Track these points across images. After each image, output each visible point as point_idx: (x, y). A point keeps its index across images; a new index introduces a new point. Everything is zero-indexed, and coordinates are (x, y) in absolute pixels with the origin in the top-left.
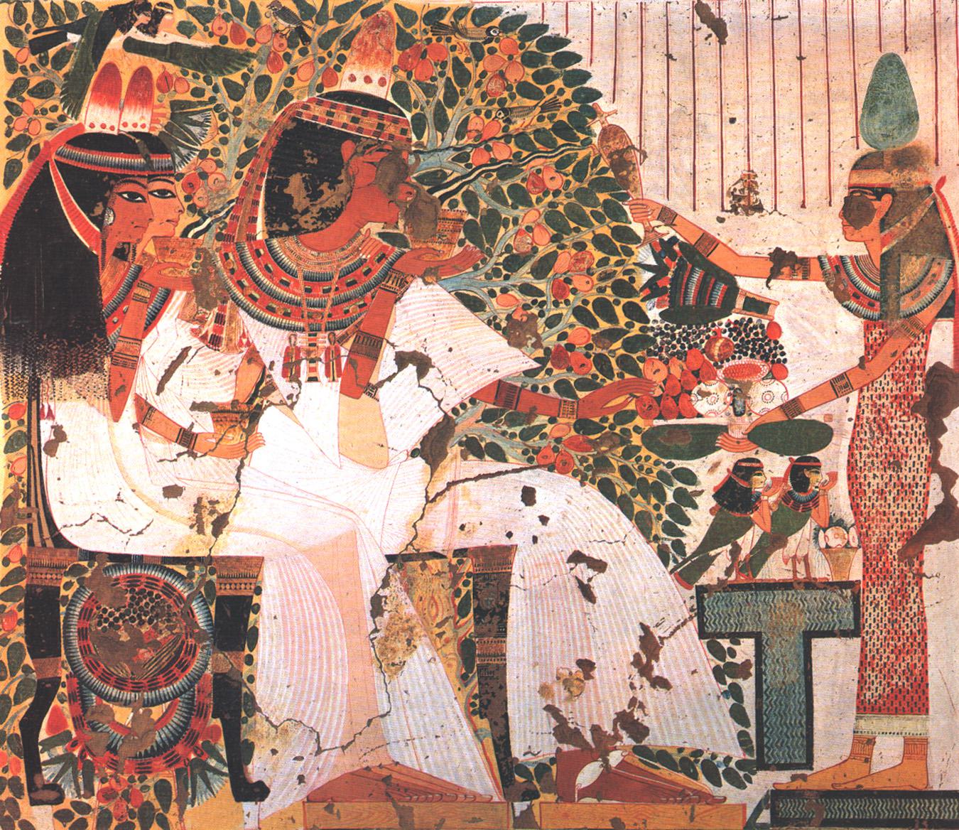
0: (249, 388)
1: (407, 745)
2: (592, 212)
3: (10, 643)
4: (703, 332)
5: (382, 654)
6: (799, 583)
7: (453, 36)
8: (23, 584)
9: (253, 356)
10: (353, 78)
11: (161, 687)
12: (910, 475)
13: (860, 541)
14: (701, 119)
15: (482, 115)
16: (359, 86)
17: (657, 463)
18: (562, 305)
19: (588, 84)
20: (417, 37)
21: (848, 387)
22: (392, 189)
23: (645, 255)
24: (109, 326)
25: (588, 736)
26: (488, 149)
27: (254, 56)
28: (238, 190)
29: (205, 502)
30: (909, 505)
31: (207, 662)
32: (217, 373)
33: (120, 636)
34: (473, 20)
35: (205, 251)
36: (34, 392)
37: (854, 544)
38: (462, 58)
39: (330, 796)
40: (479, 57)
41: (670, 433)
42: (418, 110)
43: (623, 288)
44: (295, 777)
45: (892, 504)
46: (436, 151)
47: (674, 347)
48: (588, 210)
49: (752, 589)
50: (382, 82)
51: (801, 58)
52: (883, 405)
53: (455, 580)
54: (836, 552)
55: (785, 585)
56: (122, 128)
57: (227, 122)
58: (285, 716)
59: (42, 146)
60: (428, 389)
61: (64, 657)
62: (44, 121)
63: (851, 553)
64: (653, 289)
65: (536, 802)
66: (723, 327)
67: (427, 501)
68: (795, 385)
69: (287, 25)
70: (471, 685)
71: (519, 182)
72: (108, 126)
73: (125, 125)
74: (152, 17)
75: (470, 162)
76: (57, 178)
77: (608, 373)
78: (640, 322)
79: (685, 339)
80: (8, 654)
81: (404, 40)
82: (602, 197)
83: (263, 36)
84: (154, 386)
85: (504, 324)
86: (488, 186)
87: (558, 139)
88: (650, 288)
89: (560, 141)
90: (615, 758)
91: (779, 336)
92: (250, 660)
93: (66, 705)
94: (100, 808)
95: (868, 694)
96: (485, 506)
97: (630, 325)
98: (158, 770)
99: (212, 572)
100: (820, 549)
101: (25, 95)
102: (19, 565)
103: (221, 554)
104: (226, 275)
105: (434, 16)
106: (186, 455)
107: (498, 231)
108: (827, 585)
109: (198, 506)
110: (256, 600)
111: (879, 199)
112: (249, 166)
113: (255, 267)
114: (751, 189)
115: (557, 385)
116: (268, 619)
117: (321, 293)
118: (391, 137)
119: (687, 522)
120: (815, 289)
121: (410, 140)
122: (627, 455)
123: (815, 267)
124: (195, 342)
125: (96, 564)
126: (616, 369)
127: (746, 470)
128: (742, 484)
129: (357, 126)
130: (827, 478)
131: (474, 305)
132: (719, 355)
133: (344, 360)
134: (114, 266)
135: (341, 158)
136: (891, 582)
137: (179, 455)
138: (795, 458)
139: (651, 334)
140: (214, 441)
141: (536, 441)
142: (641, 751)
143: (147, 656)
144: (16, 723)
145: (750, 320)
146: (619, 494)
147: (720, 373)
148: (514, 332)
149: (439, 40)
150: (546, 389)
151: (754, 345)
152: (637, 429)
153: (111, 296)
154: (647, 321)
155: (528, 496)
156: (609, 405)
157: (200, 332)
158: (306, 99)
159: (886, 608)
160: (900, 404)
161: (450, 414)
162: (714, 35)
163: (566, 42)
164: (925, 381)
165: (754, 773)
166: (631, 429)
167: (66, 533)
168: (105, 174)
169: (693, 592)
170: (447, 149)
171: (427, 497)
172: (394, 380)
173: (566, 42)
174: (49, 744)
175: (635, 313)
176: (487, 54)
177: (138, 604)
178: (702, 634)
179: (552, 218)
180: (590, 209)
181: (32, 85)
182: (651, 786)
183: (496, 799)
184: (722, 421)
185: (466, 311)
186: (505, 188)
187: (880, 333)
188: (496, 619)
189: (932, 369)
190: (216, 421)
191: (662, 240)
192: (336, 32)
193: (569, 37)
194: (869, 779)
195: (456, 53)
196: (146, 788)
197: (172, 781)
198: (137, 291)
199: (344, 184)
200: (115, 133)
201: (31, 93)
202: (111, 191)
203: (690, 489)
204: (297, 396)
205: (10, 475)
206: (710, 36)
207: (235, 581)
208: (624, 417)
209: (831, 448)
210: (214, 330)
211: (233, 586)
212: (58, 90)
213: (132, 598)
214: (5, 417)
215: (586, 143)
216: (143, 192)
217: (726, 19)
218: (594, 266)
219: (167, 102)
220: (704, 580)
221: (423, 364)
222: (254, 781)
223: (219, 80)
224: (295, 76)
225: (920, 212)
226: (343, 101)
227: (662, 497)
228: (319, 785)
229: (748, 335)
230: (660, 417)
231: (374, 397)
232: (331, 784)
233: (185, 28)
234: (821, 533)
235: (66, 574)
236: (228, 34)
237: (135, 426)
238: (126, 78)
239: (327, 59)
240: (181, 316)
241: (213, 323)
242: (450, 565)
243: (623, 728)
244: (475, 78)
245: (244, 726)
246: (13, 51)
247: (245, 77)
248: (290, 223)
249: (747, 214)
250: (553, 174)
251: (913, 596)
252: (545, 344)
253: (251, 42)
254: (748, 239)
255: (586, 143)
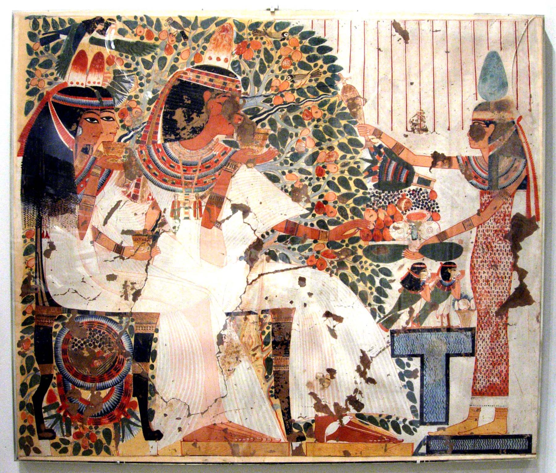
0: (153, 223)
1: (236, 412)
2: (338, 131)
3: (27, 356)
4: (395, 195)
5: (223, 365)
6: (444, 329)
7: (264, 37)
8: (33, 325)
9: (155, 206)
10: (210, 58)
11: (105, 380)
12: (502, 272)
13: (476, 307)
14: (396, 82)
15: (279, 78)
16: (214, 63)
17: (371, 265)
18: (322, 180)
19: (336, 63)
20: (245, 37)
21: (471, 226)
22: (230, 117)
23: (365, 154)
24: (78, 189)
25: (332, 409)
26: (282, 96)
27: (158, 46)
28: (148, 117)
29: (129, 283)
30: (501, 288)
31: (130, 368)
32: (136, 214)
33: (84, 353)
34: (275, 28)
35: (130, 149)
36: (39, 224)
37: (473, 307)
38: (269, 48)
39: (195, 438)
40: (278, 48)
41: (378, 248)
42: (245, 76)
43: (353, 171)
44: (177, 428)
45: (493, 287)
46: (255, 97)
47: (381, 203)
48: (335, 129)
49: (419, 332)
50: (226, 60)
51: (447, 52)
52: (489, 235)
53: (262, 326)
54: (464, 312)
55: (437, 330)
56: (87, 84)
57: (143, 81)
58: (171, 396)
59: (45, 93)
60: (249, 224)
61: (55, 364)
62: (46, 81)
63: (472, 313)
64: (370, 172)
65: (304, 442)
66: (407, 193)
67: (248, 284)
68: (444, 225)
69: (176, 30)
70: (271, 381)
71: (298, 114)
72: (80, 83)
73: (89, 82)
74: (105, 26)
75: (272, 103)
76: (52, 110)
77: (346, 216)
78: (363, 189)
79: (386, 199)
80: (26, 361)
81: (239, 39)
82: (343, 122)
83: (163, 36)
84: (102, 223)
85: (290, 190)
86: (282, 116)
87: (319, 91)
88: (368, 171)
89: (321, 93)
90: (346, 420)
91: (436, 198)
92: (152, 367)
93: (56, 388)
94: (75, 442)
95: (478, 386)
96: (281, 283)
97: (357, 191)
98: (105, 423)
99: (133, 320)
100: (455, 311)
101: (37, 67)
102: (31, 315)
103: (137, 311)
104: (141, 162)
105: (254, 26)
106: (119, 258)
107: (287, 140)
108: (460, 330)
109: (125, 286)
110: (155, 335)
111: (488, 126)
112: (154, 104)
113: (156, 158)
114: (421, 120)
115: (318, 223)
116: (161, 346)
117: (192, 172)
118: (230, 89)
119: (386, 296)
120: (455, 173)
121: (240, 91)
122: (355, 260)
123: (454, 161)
124: (124, 198)
125: (71, 315)
126: (350, 215)
127: (418, 269)
128: (415, 276)
129: (212, 83)
130: (459, 273)
131: (274, 179)
132: (405, 208)
133: (203, 208)
134: (81, 157)
135: (203, 100)
136: (491, 328)
137: (115, 258)
138: (443, 262)
139: (368, 196)
140: (134, 251)
141: (306, 253)
142: (360, 416)
143: (98, 364)
144: (30, 398)
145: (421, 189)
146: (350, 281)
147: (405, 217)
148: (295, 194)
149: (257, 39)
150: (312, 225)
151: (423, 202)
152: (360, 247)
153: (80, 174)
154: (366, 189)
155: (302, 281)
156: (346, 234)
157: (127, 192)
158: (185, 69)
159: (488, 341)
160: (498, 235)
161: (260, 238)
162: (402, 39)
163: (323, 41)
164: (511, 223)
165: (418, 427)
166: (357, 246)
167: (57, 299)
168: (78, 108)
169: (389, 333)
170: (260, 96)
171: (247, 282)
172: (230, 219)
173: (323, 41)
174: (47, 409)
175: (360, 184)
176: (282, 46)
177: (93, 337)
178: (393, 355)
179: (316, 134)
180: (337, 129)
181: (41, 61)
182: (364, 433)
183: (283, 441)
184: (406, 243)
185: (270, 183)
186: (291, 117)
187: (488, 197)
188: (284, 347)
189: (515, 216)
190: (135, 240)
191: (374, 146)
192: (202, 34)
193: (326, 38)
194: (477, 430)
195: (266, 46)
196: (98, 432)
197: (112, 430)
198: (93, 170)
199: (205, 114)
200: (84, 87)
201: (41, 66)
202: (81, 117)
203: (388, 278)
204: (178, 227)
205: (26, 268)
206: (400, 39)
207: (145, 325)
208: (353, 240)
209: (462, 257)
210: (135, 192)
211: (143, 328)
212: (54, 65)
213: (90, 334)
214: (23, 237)
215: (334, 94)
216: (97, 117)
217: (408, 31)
218: (338, 159)
219: (111, 70)
220: (394, 327)
221: (246, 211)
222: (155, 430)
223: (139, 59)
224: (179, 57)
225: (509, 134)
226: (205, 70)
227: (373, 282)
228: (189, 433)
229: (419, 198)
230: (373, 240)
231: (219, 228)
232: (196, 432)
233: (121, 32)
234: (456, 302)
235: (56, 320)
236: (144, 35)
237: (92, 242)
238: (90, 58)
239: (197, 48)
240: (117, 184)
241: (134, 188)
242: (260, 318)
243: (350, 404)
244: (276, 59)
245: (149, 401)
246: (31, 44)
247: (153, 57)
248: (176, 135)
249: (420, 133)
250: (317, 110)
251: (502, 335)
252: (312, 200)
253: (157, 39)
254: (420, 148)
255: (334, 94)
